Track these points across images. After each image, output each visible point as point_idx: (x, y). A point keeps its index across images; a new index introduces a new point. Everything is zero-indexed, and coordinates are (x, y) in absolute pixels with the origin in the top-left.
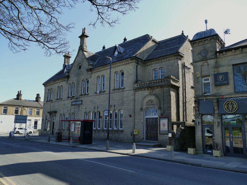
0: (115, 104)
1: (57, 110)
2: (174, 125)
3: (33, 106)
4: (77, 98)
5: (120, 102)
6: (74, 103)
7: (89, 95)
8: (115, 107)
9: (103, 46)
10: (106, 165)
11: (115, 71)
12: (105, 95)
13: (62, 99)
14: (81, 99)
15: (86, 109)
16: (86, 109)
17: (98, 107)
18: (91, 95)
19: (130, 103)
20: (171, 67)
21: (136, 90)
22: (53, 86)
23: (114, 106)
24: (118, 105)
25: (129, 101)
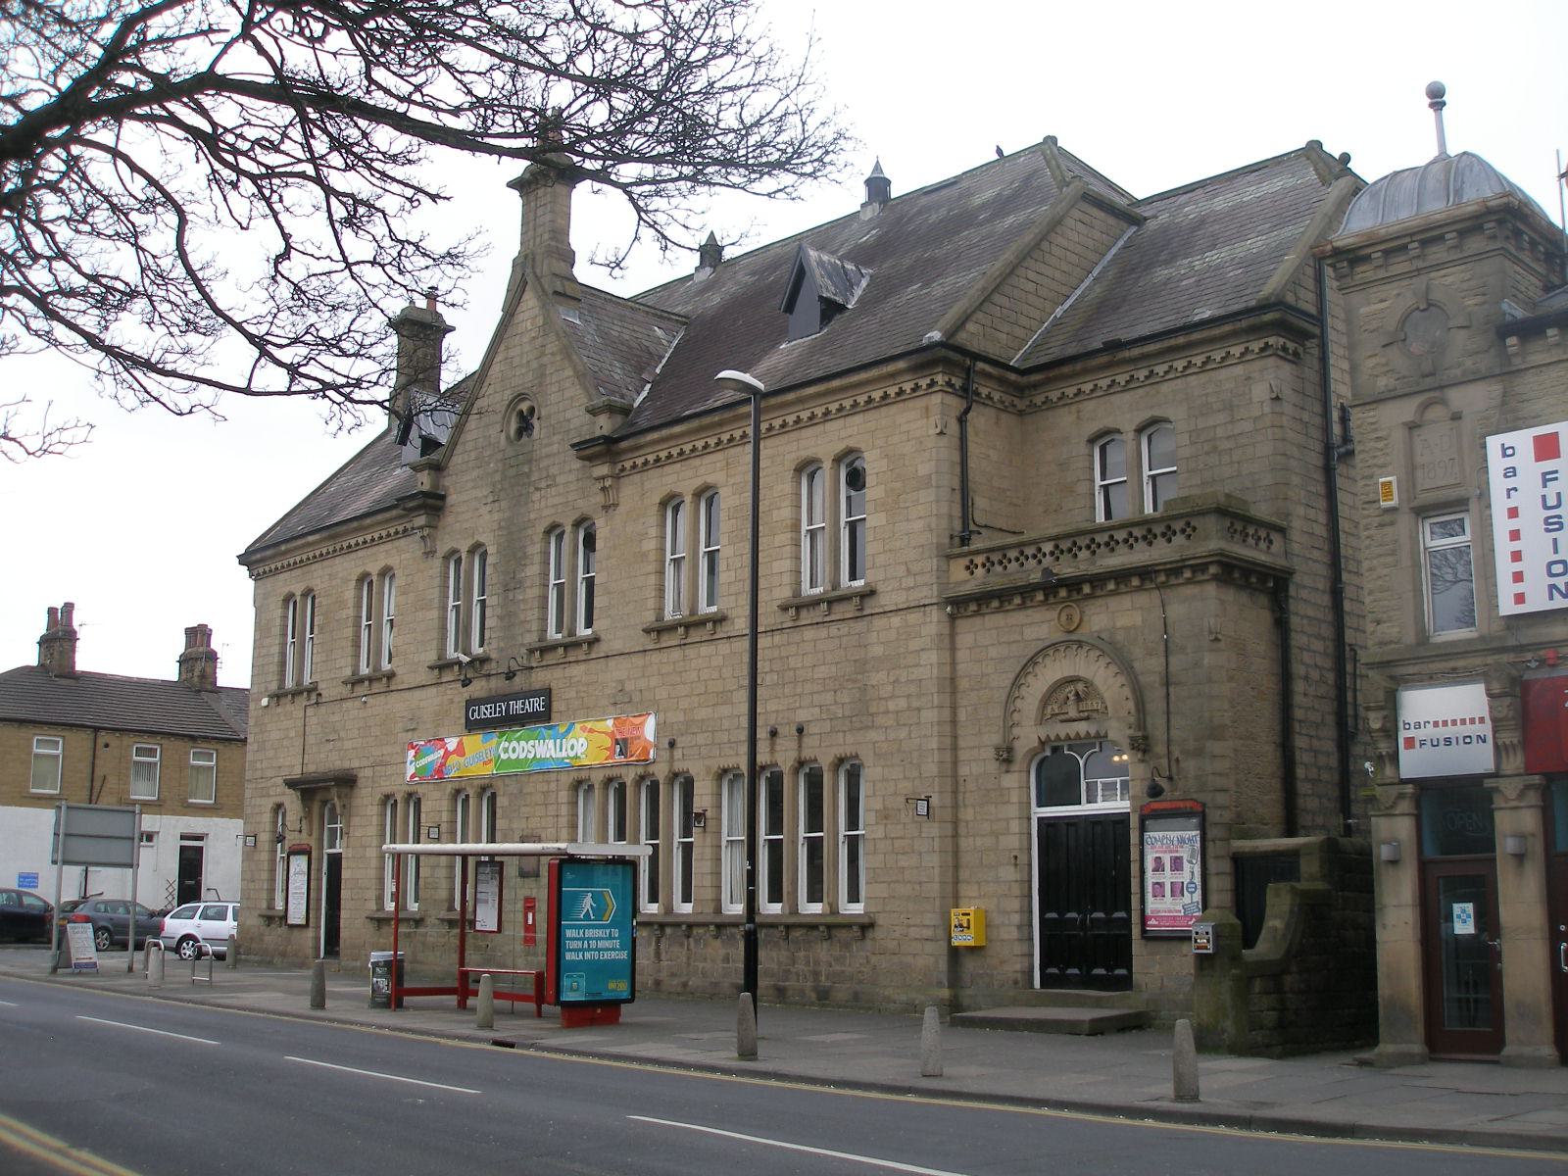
1: (355, 764)
4: (510, 675)
6: (486, 712)
8: (806, 740)
11: (793, 456)
13: (391, 676)
14: (539, 679)
19: (919, 709)
21: (960, 606)
22: (318, 577)
24: (827, 726)
25: (913, 689)
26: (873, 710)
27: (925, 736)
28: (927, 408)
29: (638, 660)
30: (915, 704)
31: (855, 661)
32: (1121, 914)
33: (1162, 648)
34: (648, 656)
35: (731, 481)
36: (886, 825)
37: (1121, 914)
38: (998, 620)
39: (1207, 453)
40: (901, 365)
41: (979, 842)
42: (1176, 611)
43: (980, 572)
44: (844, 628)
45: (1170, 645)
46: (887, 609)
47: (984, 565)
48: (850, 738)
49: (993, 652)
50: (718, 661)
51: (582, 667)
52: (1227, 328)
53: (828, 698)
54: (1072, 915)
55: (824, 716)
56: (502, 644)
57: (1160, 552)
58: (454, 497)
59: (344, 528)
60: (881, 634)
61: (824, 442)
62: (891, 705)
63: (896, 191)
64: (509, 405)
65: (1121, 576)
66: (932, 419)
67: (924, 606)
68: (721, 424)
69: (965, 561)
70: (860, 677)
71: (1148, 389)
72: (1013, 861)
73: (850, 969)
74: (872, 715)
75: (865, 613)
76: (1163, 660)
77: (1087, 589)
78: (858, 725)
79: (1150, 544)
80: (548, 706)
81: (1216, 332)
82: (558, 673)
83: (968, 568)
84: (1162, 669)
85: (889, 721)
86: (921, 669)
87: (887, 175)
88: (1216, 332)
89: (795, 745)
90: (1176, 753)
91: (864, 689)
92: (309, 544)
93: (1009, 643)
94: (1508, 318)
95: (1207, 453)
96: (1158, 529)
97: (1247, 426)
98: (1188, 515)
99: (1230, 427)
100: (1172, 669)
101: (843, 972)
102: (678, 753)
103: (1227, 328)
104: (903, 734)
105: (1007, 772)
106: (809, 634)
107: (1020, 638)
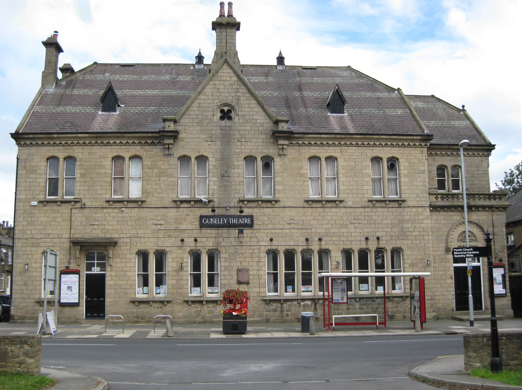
0: (378, 234)
1: (116, 236)
2: (495, 293)
3: (222, 208)
5: (395, 230)
7: (281, 204)
8: (380, 242)
9: (277, 56)
10: (470, 296)
11: (370, 154)
12: (343, 210)
15: (271, 240)
16: (271, 240)
17: (320, 240)
18: (350, 204)
19: (424, 236)
20: (475, 169)
23: (378, 238)
24: (389, 238)
25: (421, 230)
26: (407, 234)
27: (426, 243)
28: (422, 151)
29: (302, 210)
30: (422, 234)
31: (399, 220)
32: (102, 299)
33: (492, 226)
34: (306, 209)
35: (343, 157)
36: (412, 268)
37: (102, 299)
38: (445, 213)
39: (472, 177)
40: (419, 138)
41: (440, 273)
42: (495, 217)
43: (439, 199)
44: (394, 210)
45: (494, 225)
46: (410, 206)
47: (440, 198)
48: (398, 242)
49: (443, 222)
50: (341, 214)
51: (271, 210)
52: (481, 148)
53: (390, 230)
54: (95, 299)
55: (387, 235)
56: (221, 196)
57: (493, 202)
58: (183, 135)
59: (110, 135)
60: (407, 213)
61: (385, 153)
62: (413, 234)
63: (287, 63)
64: (219, 106)
65: (484, 207)
66: (424, 155)
67: (424, 207)
68: (342, 138)
69: (435, 196)
70: (401, 224)
71: (455, 157)
72: (451, 278)
73: (401, 310)
74: (406, 236)
75: (402, 206)
76: (492, 229)
77: (473, 209)
78: (401, 238)
79: (490, 200)
80: (252, 221)
81: (478, 148)
82: (256, 210)
83: (435, 198)
84: (492, 231)
85: (413, 238)
86: (424, 224)
87: (284, 55)
88: (478, 148)
89: (376, 243)
90: (496, 252)
91: (402, 228)
92: (78, 137)
93: (448, 220)
94: (102, 95)
95: (472, 177)
96: (492, 197)
97: (482, 172)
98: (501, 195)
99: (477, 171)
100: (494, 231)
101: (398, 310)
102: (323, 243)
103: (481, 148)
104: (418, 242)
105: (448, 254)
106: (379, 210)
107: (451, 219)
